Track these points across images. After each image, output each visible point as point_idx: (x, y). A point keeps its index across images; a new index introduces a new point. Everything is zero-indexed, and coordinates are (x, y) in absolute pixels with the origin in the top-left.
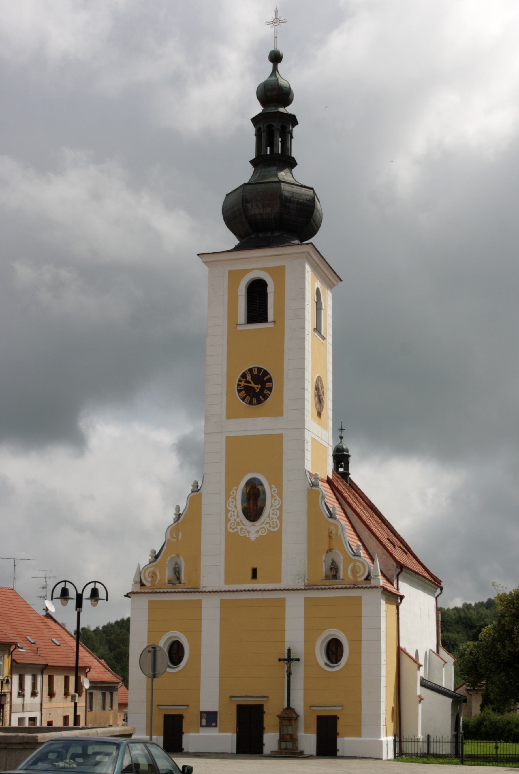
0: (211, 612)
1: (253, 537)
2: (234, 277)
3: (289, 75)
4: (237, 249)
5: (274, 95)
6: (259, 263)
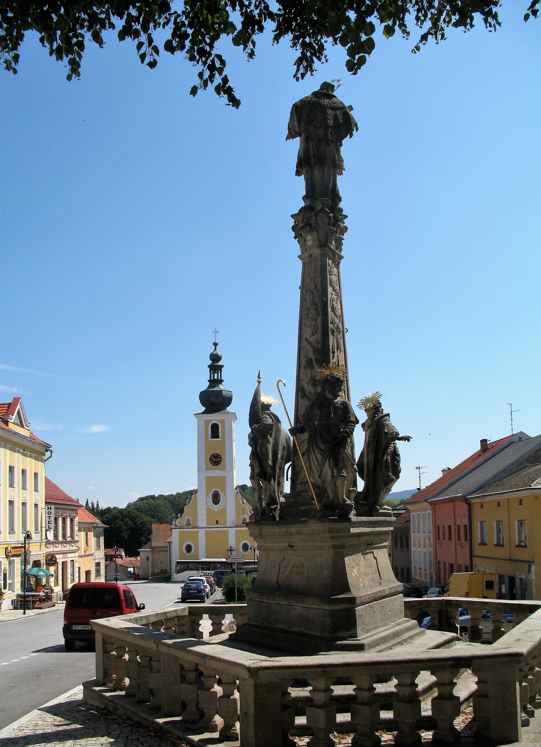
0: (202, 534)
1: (216, 510)
2: (207, 422)
3: (418, 42)
5: (215, 358)
6: (214, 418)
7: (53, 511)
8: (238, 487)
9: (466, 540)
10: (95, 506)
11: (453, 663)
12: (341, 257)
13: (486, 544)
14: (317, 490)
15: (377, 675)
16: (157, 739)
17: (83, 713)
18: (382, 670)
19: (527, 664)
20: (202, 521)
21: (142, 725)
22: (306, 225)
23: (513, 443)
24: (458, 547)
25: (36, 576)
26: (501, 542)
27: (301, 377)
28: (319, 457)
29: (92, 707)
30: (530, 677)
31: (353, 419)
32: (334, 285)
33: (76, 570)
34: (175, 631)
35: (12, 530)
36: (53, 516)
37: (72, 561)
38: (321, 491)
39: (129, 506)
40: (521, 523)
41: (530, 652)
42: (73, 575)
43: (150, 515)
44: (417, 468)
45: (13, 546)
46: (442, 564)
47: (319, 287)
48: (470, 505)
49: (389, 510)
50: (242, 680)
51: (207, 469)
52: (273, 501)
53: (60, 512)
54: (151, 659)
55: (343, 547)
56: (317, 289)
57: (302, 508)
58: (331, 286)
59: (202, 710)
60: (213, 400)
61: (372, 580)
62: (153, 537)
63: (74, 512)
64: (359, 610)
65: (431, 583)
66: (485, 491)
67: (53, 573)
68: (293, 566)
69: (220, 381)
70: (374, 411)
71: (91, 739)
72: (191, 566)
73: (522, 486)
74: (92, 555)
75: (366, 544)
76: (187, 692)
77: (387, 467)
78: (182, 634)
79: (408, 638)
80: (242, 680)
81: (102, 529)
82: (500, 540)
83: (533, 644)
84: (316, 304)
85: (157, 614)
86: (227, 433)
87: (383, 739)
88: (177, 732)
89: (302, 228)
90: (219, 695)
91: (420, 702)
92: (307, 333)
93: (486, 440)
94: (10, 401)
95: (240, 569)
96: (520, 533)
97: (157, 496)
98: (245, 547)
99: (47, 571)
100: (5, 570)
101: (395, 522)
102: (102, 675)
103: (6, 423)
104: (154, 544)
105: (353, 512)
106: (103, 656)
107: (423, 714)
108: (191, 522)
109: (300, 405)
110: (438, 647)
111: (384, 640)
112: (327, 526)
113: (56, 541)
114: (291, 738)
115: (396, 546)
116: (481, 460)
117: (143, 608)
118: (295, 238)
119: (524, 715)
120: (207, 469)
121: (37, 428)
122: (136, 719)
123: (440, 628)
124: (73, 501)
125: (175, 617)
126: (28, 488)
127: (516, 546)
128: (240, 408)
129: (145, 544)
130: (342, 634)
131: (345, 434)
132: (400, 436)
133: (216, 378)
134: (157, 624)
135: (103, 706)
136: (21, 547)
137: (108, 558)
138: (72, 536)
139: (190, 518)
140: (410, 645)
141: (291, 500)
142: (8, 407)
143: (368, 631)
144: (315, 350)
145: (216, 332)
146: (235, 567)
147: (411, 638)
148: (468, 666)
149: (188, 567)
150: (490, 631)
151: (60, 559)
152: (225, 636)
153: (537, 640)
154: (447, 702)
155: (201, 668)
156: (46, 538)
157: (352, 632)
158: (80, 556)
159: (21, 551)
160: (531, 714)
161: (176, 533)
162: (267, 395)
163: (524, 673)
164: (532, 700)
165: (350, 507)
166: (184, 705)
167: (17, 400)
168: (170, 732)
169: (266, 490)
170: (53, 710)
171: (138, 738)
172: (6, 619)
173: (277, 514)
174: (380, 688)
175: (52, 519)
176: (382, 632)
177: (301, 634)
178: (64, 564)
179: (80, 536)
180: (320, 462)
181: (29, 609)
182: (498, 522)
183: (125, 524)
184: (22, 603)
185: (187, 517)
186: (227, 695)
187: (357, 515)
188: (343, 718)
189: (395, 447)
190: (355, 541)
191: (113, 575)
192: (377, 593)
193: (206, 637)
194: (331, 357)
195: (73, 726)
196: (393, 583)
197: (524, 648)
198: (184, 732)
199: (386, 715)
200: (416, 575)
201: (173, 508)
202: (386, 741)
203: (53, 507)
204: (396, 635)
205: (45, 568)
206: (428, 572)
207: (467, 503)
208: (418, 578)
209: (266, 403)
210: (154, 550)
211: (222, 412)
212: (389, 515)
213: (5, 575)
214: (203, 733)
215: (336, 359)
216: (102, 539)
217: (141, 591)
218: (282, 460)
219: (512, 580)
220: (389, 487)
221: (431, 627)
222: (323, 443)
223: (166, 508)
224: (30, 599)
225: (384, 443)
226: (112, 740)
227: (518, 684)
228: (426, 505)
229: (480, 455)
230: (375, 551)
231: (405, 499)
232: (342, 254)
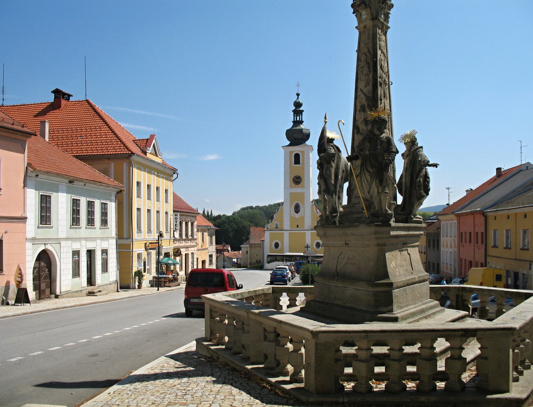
0: (286, 235)
1: (297, 217)
2: (291, 152)
4: (289, 145)
5: (298, 105)
6: (297, 149)
7: (178, 217)
8: (314, 200)
9: (482, 243)
10: (210, 214)
11: (463, 333)
12: (388, 28)
13: (497, 247)
14: (366, 203)
15: (405, 340)
16: (246, 379)
17: (196, 360)
18: (410, 337)
19: (520, 336)
20: (287, 225)
21: (236, 370)
22: (361, 3)
23: (521, 171)
24: (476, 249)
25: (166, 264)
26: (509, 246)
27: (357, 119)
28: (369, 178)
29: (202, 356)
30: (522, 346)
31: (394, 150)
32: (382, 48)
33: (195, 260)
34: (262, 304)
35: (149, 231)
36: (178, 221)
37: (192, 253)
38: (369, 204)
39: (234, 214)
40: (525, 232)
41: (522, 328)
42: (193, 263)
43: (249, 220)
44: (447, 188)
45: (150, 242)
46: (463, 261)
47: (371, 51)
48: (486, 217)
49: (420, 218)
50: (307, 340)
51: (291, 187)
52: (334, 210)
53: (184, 218)
54: (243, 324)
55: (385, 245)
56: (369, 51)
57: (356, 216)
58: (380, 49)
59: (278, 360)
60: (296, 136)
61: (406, 270)
62: (251, 237)
63: (194, 218)
64: (395, 292)
65: (455, 275)
66: (498, 207)
67: (178, 261)
68: (348, 259)
69: (301, 122)
70: (410, 144)
71: (200, 378)
72: (278, 258)
73: (527, 204)
74: (207, 249)
75: (402, 244)
76: (268, 347)
77: (419, 186)
78: (267, 306)
79: (432, 314)
80: (307, 340)
81: (214, 231)
82: (508, 244)
83: (524, 321)
84: (368, 63)
85: (249, 292)
86: (306, 163)
87: (408, 386)
88: (260, 376)
89: (359, 5)
90: (290, 350)
91: (436, 361)
92: (362, 85)
93: (500, 168)
94: (148, 137)
95: (314, 261)
96: (524, 239)
97: (254, 206)
98: (318, 245)
99: (174, 261)
100: (145, 259)
101: (425, 228)
102: (209, 334)
103: (145, 153)
104: (252, 241)
105: (393, 219)
106: (210, 321)
107: (439, 369)
108: (279, 226)
109: (355, 139)
110: (453, 321)
111: (413, 314)
112: (373, 229)
113: (181, 239)
114: (341, 383)
115: (429, 247)
116: (496, 183)
117: (242, 287)
118: (354, 13)
119: (515, 373)
120: (291, 187)
121: (167, 156)
122: (232, 366)
123: (457, 307)
124: (193, 210)
125: (262, 294)
126: (161, 200)
127: (521, 249)
128: (313, 142)
129: (245, 241)
130: (382, 309)
131: (388, 161)
132: (430, 163)
133: (298, 119)
134: (249, 299)
135: (209, 356)
136: (156, 243)
137: (218, 251)
138: (192, 235)
139: (278, 223)
140: (432, 319)
141: (348, 210)
142: (147, 142)
143: (401, 308)
144: (367, 98)
145: (298, 85)
146: (310, 259)
147: (434, 314)
148: (474, 336)
149: (276, 259)
150: (494, 312)
151: (183, 251)
152: (297, 309)
153: (529, 317)
154: (457, 361)
155: (278, 331)
156: (174, 236)
157: (389, 308)
158: (198, 250)
159: (157, 246)
160: (521, 373)
161: (267, 234)
162: (331, 131)
163: (516, 343)
164: (522, 363)
165: (390, 216)
166: (266, 357)
167: (152, 137)
168: (255, 375)
169: (329, 202)
170: (173, 357)
171: (233, 379)
172: (145, 294)
173: (337, 220)
174: (408, 349)
175: (178, 223)
176: (412, 309)
177: (352, 308)
178: (186, 255)
179: (198, 235)
180: (369, 182)
181: (161, 287)
182: (507, 231)
183: (231, 227)
184: (157, 283)
185: (276, 222)
186: (296, 350)
187: (396, 221)
188: (379, 369)
189: (426, 171)
190: (394, 241)
191: (221, 264)
192: (409, 280)
193: (284, 308)
194: (379, 103)
195: (188, 369)
196: (421, 272)
197: (517, 325)
198: (265, 375)
199: (411, 369)
200: (443, 268)
201: (266, 216)
202: (410, 388)
203: (178, 214)
204: (422, 311)
205: (173, 258)
206: (453, 267)
207: (484, 216)
208: (445, 271)
209: (330, 137)
210: (251, 246)
211: (303, 145)
212: (420, 222)
213: (145, 263)
214: (278, 376)
215: (383, 105)
216: (214, 238)
217: (240, 276)
218: (342, 180)
219: (516, 275)
220: (421, 201)
221: (450, 307)
222: (372, 168)
223: (261, 215)
224: (163, 280)
225: (418, 168)
226: (215, 379)
227: (511, 350)
228: (452, 216)
229: (496, 179)
230: (409, 249)
231: (438, 212)
232: (389, 25)
